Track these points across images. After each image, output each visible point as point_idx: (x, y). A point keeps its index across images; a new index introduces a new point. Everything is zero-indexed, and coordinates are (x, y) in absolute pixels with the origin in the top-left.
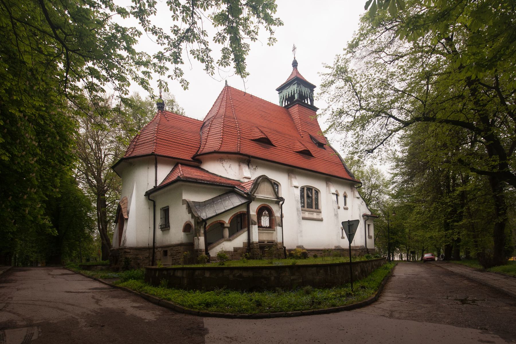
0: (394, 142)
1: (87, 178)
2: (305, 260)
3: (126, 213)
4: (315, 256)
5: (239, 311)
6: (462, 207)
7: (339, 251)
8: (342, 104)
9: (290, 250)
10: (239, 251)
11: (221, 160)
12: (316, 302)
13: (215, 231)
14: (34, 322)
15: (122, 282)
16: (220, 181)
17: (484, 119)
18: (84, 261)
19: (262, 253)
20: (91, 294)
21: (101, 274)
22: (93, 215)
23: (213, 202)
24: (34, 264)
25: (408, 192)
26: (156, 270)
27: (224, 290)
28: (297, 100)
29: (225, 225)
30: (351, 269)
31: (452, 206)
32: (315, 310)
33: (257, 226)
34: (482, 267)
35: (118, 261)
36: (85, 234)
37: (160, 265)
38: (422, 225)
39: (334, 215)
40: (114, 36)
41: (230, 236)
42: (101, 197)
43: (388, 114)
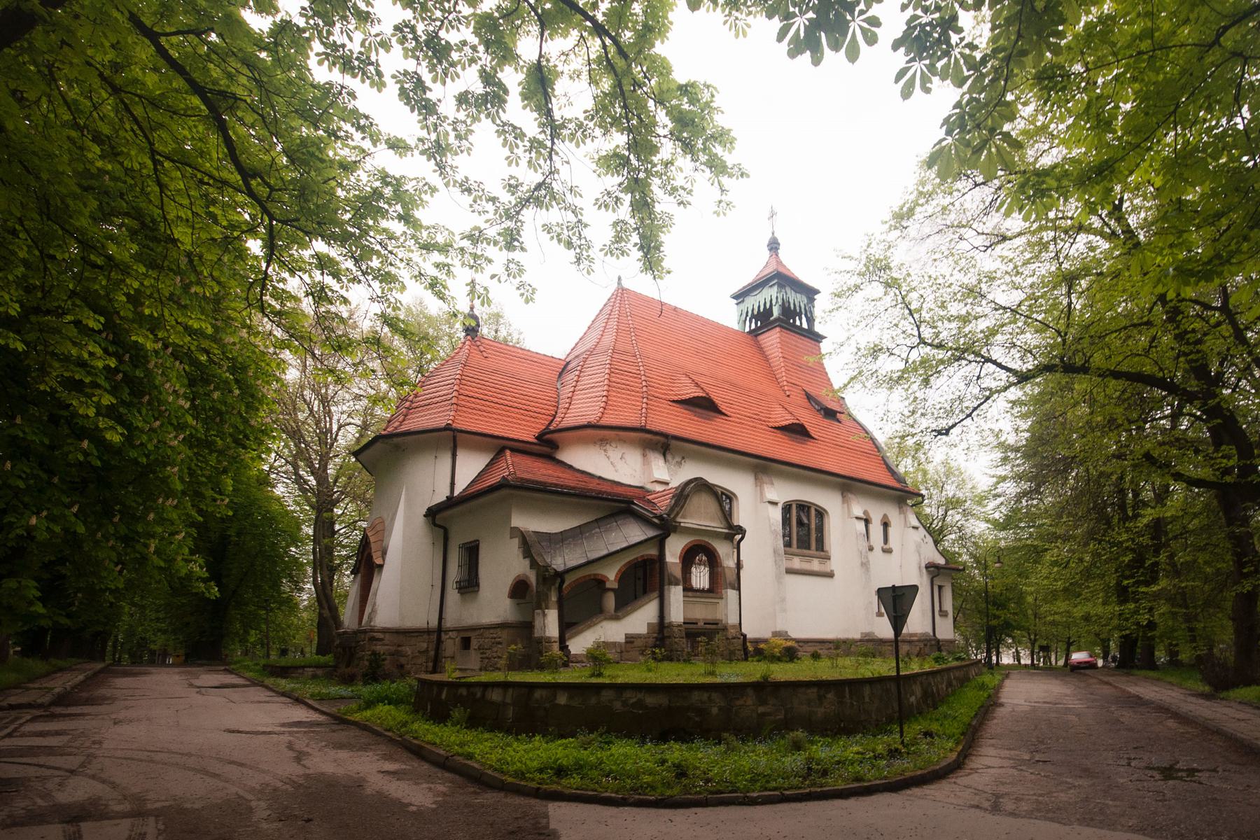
0: (995, 413)
1: (296, 474)
2: (791, 665)
3: (379, 553)
4: (816, 656)
5: (634, 789)
6: (1157, 552)
7: (870, 645)
8: (878, 333)
9: (756, 641)
10: (638, 643)
11: (603, 442)
12: (817, 771)
13: (583, 598)
14: (149, 806)
15: (360, 709)
16: (599, 487)
17: (1200, 371)
18: (274, 656)
19: (693, 647)
20: (286, 738)
21: (313, 688)
22: (304, 553)
23: (581, 533)
24: (158, 659)
25: (1031, 517)
26: (441, 685)
27: (601, 735)
28: (776, 320)
29: (608, 585)
30: (899, 693)
31: (1133, 550)
32: (812, 788)
33: (680, 588)
34: (1207, 689)
35: (350, 658)
36: (280, 592)
37: (449, 674)
38: (1065, 590)
39: (859, 564)
40: (377, 194)
41: (617, 608)
42: (325, 515)
43: (983, 357)
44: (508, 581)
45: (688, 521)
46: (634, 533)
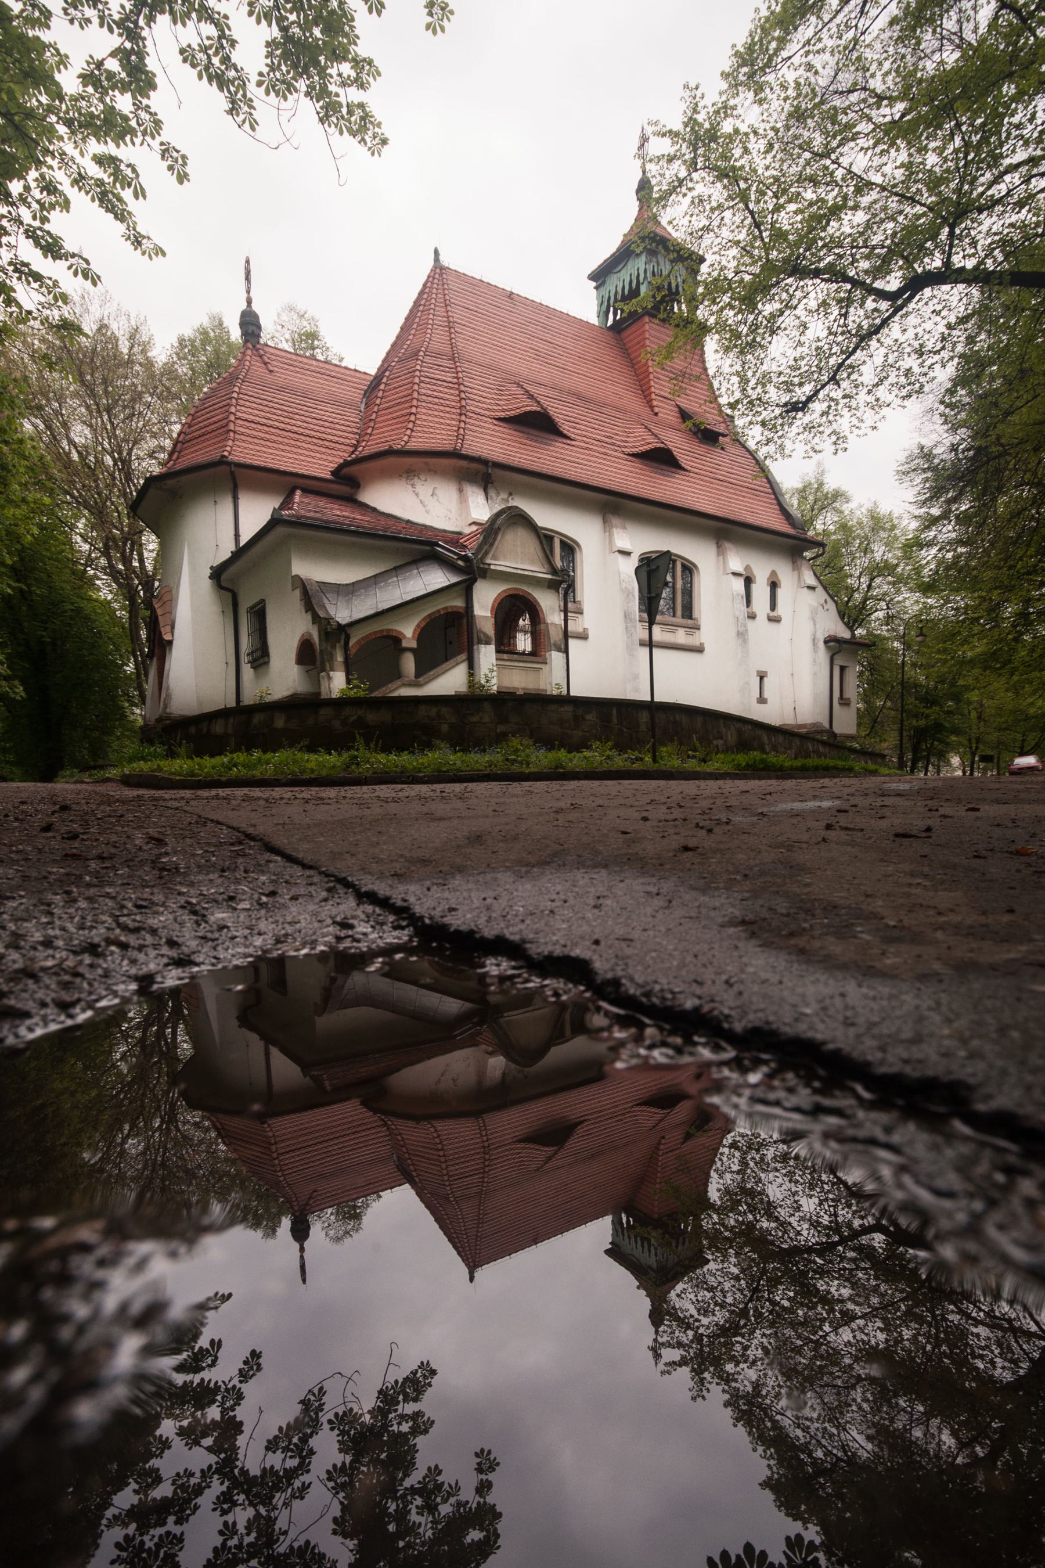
3: (168, 628)
11: (409, 474)
29: (405, 644)
39: (734, 633)
41: (419, 673)
44: (294, 644)
45: (501, 563)
46: (436, 578)
